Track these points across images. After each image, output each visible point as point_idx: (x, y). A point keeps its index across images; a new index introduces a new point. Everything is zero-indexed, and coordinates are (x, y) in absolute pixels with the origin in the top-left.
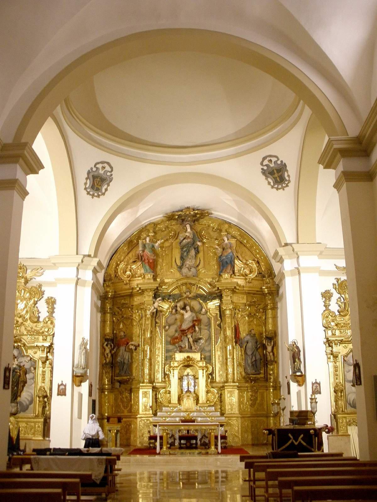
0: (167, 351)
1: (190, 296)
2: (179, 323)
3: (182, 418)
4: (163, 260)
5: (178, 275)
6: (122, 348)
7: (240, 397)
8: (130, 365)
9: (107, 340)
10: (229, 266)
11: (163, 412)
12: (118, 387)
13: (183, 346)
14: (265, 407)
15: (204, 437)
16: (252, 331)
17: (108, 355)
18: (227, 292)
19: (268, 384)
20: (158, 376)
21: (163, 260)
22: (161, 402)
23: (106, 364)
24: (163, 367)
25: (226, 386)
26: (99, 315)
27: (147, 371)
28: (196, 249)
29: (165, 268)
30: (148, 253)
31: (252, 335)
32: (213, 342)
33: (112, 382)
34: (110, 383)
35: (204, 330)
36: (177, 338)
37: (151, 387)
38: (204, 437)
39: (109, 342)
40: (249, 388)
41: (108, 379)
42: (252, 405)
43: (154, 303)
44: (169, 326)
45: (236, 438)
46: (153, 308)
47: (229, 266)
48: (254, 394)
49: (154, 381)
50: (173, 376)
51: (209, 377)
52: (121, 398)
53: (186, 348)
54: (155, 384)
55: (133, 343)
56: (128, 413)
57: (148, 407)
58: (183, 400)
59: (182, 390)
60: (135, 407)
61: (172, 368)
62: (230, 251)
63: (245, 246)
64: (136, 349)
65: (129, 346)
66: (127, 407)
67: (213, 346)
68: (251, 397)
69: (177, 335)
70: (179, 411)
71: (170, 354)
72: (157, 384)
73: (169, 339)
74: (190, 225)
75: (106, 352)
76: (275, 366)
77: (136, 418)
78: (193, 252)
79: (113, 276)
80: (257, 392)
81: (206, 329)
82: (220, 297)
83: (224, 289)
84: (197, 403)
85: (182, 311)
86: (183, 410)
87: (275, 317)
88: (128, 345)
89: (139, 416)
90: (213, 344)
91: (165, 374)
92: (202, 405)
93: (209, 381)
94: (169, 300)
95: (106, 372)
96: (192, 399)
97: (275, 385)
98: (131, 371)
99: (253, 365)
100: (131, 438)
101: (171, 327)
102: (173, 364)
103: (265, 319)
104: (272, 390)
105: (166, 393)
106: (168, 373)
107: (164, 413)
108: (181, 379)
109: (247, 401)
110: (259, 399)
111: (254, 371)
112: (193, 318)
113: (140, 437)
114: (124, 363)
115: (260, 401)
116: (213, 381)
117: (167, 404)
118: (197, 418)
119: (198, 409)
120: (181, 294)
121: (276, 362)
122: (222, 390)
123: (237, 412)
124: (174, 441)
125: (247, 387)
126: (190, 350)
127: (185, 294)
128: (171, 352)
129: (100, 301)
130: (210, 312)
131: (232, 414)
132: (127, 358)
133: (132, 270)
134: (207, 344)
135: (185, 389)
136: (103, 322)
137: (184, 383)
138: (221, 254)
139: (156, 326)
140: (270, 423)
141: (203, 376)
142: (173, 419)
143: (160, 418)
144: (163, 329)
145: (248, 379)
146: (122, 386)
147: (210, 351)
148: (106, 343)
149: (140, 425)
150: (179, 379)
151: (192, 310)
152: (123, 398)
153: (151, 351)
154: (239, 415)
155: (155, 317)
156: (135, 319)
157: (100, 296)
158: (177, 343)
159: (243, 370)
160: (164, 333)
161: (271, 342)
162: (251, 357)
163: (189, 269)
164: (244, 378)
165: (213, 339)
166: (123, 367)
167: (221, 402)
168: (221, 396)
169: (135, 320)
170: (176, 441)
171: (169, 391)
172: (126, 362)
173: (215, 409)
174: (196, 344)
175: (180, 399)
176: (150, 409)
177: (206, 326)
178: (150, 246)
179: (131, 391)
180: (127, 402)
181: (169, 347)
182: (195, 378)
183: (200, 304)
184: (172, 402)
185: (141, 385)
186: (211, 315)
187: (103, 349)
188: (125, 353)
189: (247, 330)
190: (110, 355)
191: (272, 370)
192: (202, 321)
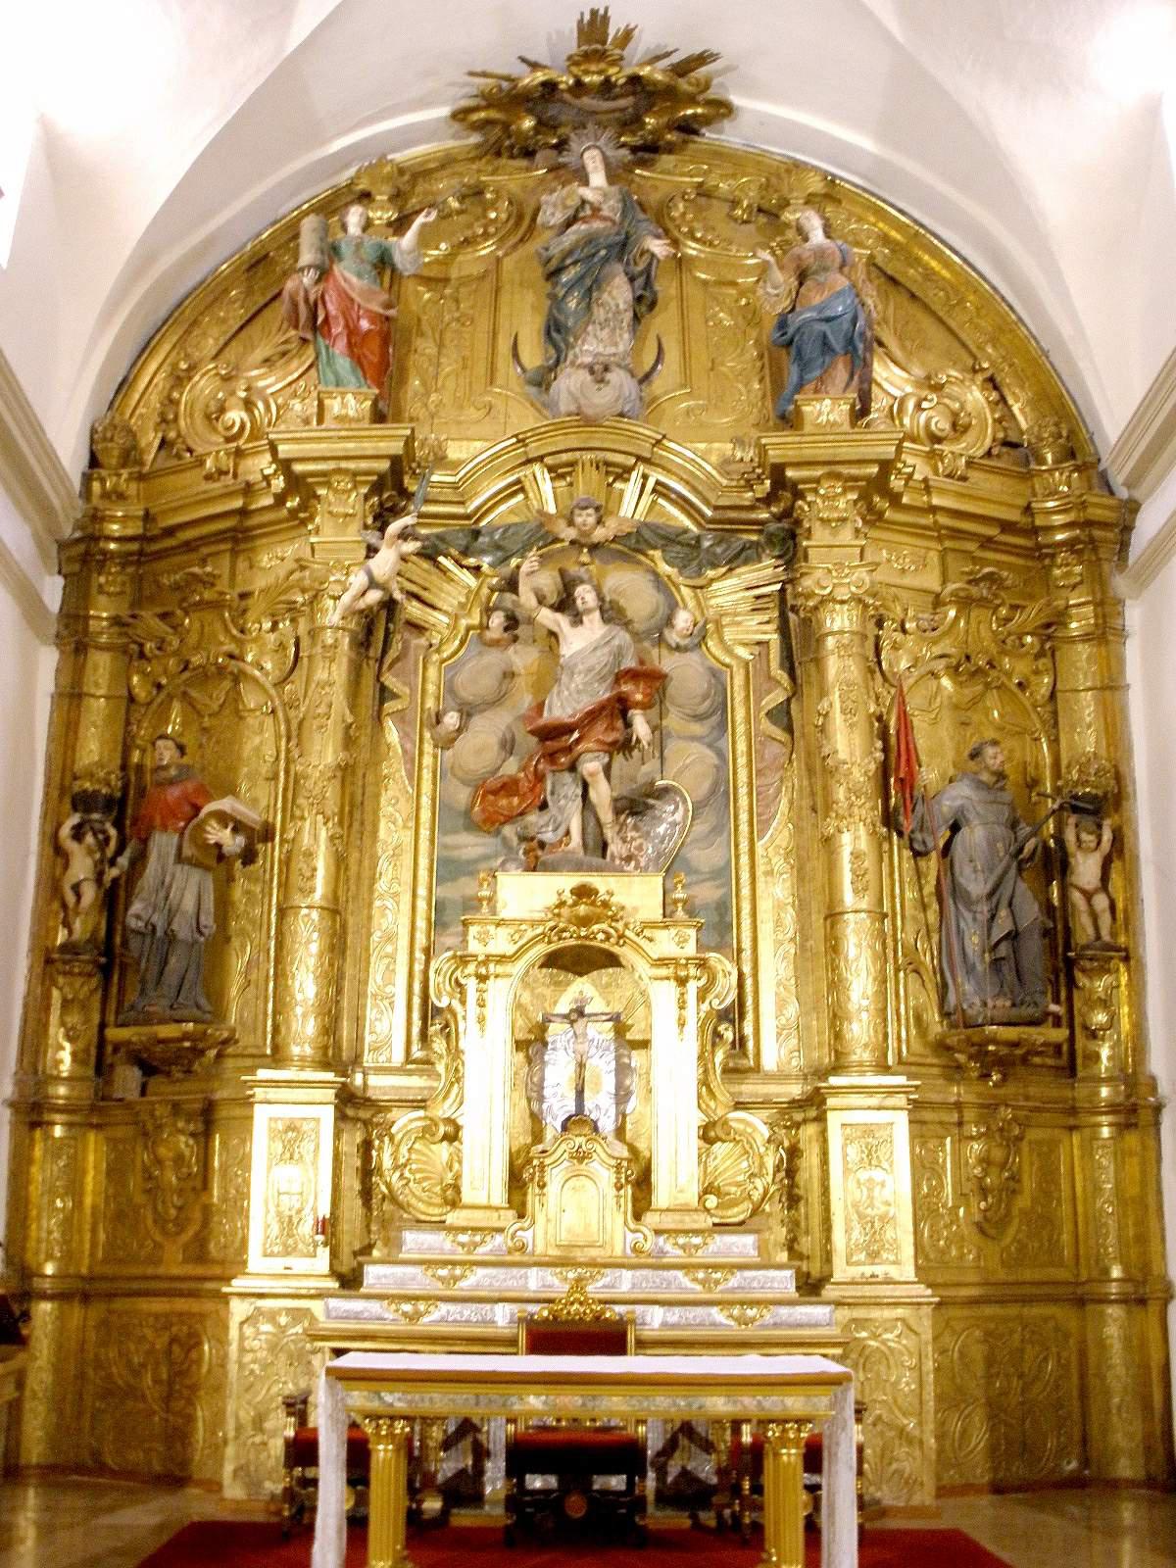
0: (448, 869)
1: (599, 534)
2: (527, 701)
3: (533, 1308)
4: (441, 346)
5: (525, 419)
6: (163, 844)
7: (923, 1168)
8: (214, 947)
9: (83, 802)
10: (840, 366)
11: (368, 1297)
12: (132, 1094)
13: (548, 836)
14: (1066, 1238)
15: (683, 1441)
16: (990, 751)
17: (78, 896)
18: (836, 497)
19: (1081, 1091)
20: (381, 1028)
21: (441, 346)
22: (392, 1198)
23: (68, 948)
24: (418, 967)
25: (838, 1091)
26: (48, 660)
27: (305, 985)
28: (640, 281)
29: (451, 384)
30: (354, 280)
31: (985, 777)
32: (744, 817)
33: (100, 1060)
34: (91, 1072)
35: (682, 744)
36: (508, 787)
37: (330, 1094)
38: (683, 1441)
39: (96, 816)
40: (969, 1115)
41: (81, 1044)
42: (988, 1227)
43: (372, 551)
44: (467, 712)
45: (901, 1451)
46: (358, 580)
47: (840, 366)
48: (998, 1154)
49: (357, 1060)
50: (481, 1020)
51: (717, 1035)
52: (146, 1170)
53: (573, 845)
54: (358, 1079)
55: (225, 804)
56: (186, 1261)
57: (306, 1228)
58: (542, 1186)
59: (536, 1120)
60: (223, 1225)
61: (471, 968)
62: (841, 282)
63: (913, 296)
64: (249, 856)
65: (200, 828)
66: (181, 1225)
67: (744, 846)
68: (985, 1171)
69: (511, 767)
70: (517, 1257)
71: (466, 887)
72: (374, 1080)
73: (462, 796)
74: (603, 153)
75: (69, 872)
76: (1124, 979)
77: (225, 1298)
78: (619, 293)
79: (150, 439)
80: (1020, 1138)
81: (693, 738)
82: (788, 543)
83: (818, 481)
84: (641, 1204)
85: (547, 617)
86: (539, 1249)
87: (1111, 686)
88: (195, 821)
89: (238, 1284)
90: (744, 828)
91: (429, 1012)
92: (669, 1221)
93: (720, 1056)
94: (472, 561)
95: (66, 1004)
96: (606, 1177)
97: (1128, 1096)
98: (217, 998)
99: (996, 964)
100: (195, 1429)
101: (477, 722)
102: (483, 940)
103: (1053, 696)
104: (1106, 1132)
105: (427, 1132)
106: (443, 1003)
107: (410, 1270)
108: (532, 1044)
109: (961, 1196)
110: (1029, 1184)
111: (1008, 1003)
112: (619, 654)
113: (239, 1428)
114: (170, 938)
115: (1034, 1200)
116: (740, 1062)
117: (435, 1212)
118: (639, 1309)
119: (647, 1246)
120: (541, 525)
121: (1126, 959)
122: (797, 1125)
123: (908, 1272)
124: (479, 1471)
125: (958, 1106)
126: (597, 861)
127: (571, 523)
128: (472, 874)
129: (60, 581)
130: (722, 640)
131: (872, 1281)
132: (189, 904)
133: (260, 405)
134: (701, 828)
135: (559, 1104)
136: (71, 696)
137: (549, 1072)
138: (786, 303)
139: (378, 718)
140: (1102, 1345)
141: (682, 1024)
142: (468, 1311)
143: (374, 1307)
144: (427, 735)
145: (961, 1058)
146: (157, 1083)
147: (722, 874)
148: (75, 819)
149: (242, 1350)
150: (520, 1045)
151: (612, 613)
152: (159, 1162)
153: (340, 862)
154: (922, 1290)
155: (381, 661)
156: (257, 673)
157: (63, 546)
158: (509, 819)
159: (934, 997)
160: (427, 760)
161: (1100, 826)
162: (984, 909)
163: (599, 372)
164: (942, 1047)
165: (743, 802)
166: (165, 962)
167: (793, 1200)
168: (790, 1168)
169: (255, 680)
170: (489, 1465)
171: (449, 1121)
172: (182, 929)
173: (761, 1248)
174: (636, 828)
175: (519, 1180)
176: (320, 1238)
177: (699, 718)
178: (369, 253)
179: (207, 1119)
180: (181, 1192)
181: (457, 847)
182: (628, 1040)
183: (659, 582)
184: (467, 1197)
185: (263, 1074)
186: (729, 651)
187: (56, 852)
188: (181, 872)
189: (950, 755)
190: (89, 893)
191: (1105, 1003)
192: (671, 690)
